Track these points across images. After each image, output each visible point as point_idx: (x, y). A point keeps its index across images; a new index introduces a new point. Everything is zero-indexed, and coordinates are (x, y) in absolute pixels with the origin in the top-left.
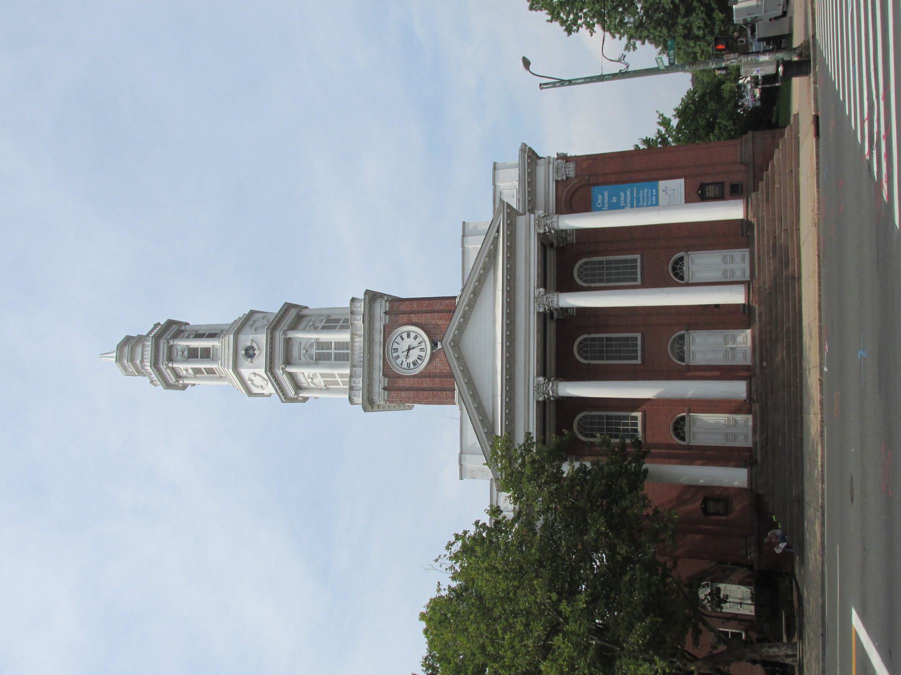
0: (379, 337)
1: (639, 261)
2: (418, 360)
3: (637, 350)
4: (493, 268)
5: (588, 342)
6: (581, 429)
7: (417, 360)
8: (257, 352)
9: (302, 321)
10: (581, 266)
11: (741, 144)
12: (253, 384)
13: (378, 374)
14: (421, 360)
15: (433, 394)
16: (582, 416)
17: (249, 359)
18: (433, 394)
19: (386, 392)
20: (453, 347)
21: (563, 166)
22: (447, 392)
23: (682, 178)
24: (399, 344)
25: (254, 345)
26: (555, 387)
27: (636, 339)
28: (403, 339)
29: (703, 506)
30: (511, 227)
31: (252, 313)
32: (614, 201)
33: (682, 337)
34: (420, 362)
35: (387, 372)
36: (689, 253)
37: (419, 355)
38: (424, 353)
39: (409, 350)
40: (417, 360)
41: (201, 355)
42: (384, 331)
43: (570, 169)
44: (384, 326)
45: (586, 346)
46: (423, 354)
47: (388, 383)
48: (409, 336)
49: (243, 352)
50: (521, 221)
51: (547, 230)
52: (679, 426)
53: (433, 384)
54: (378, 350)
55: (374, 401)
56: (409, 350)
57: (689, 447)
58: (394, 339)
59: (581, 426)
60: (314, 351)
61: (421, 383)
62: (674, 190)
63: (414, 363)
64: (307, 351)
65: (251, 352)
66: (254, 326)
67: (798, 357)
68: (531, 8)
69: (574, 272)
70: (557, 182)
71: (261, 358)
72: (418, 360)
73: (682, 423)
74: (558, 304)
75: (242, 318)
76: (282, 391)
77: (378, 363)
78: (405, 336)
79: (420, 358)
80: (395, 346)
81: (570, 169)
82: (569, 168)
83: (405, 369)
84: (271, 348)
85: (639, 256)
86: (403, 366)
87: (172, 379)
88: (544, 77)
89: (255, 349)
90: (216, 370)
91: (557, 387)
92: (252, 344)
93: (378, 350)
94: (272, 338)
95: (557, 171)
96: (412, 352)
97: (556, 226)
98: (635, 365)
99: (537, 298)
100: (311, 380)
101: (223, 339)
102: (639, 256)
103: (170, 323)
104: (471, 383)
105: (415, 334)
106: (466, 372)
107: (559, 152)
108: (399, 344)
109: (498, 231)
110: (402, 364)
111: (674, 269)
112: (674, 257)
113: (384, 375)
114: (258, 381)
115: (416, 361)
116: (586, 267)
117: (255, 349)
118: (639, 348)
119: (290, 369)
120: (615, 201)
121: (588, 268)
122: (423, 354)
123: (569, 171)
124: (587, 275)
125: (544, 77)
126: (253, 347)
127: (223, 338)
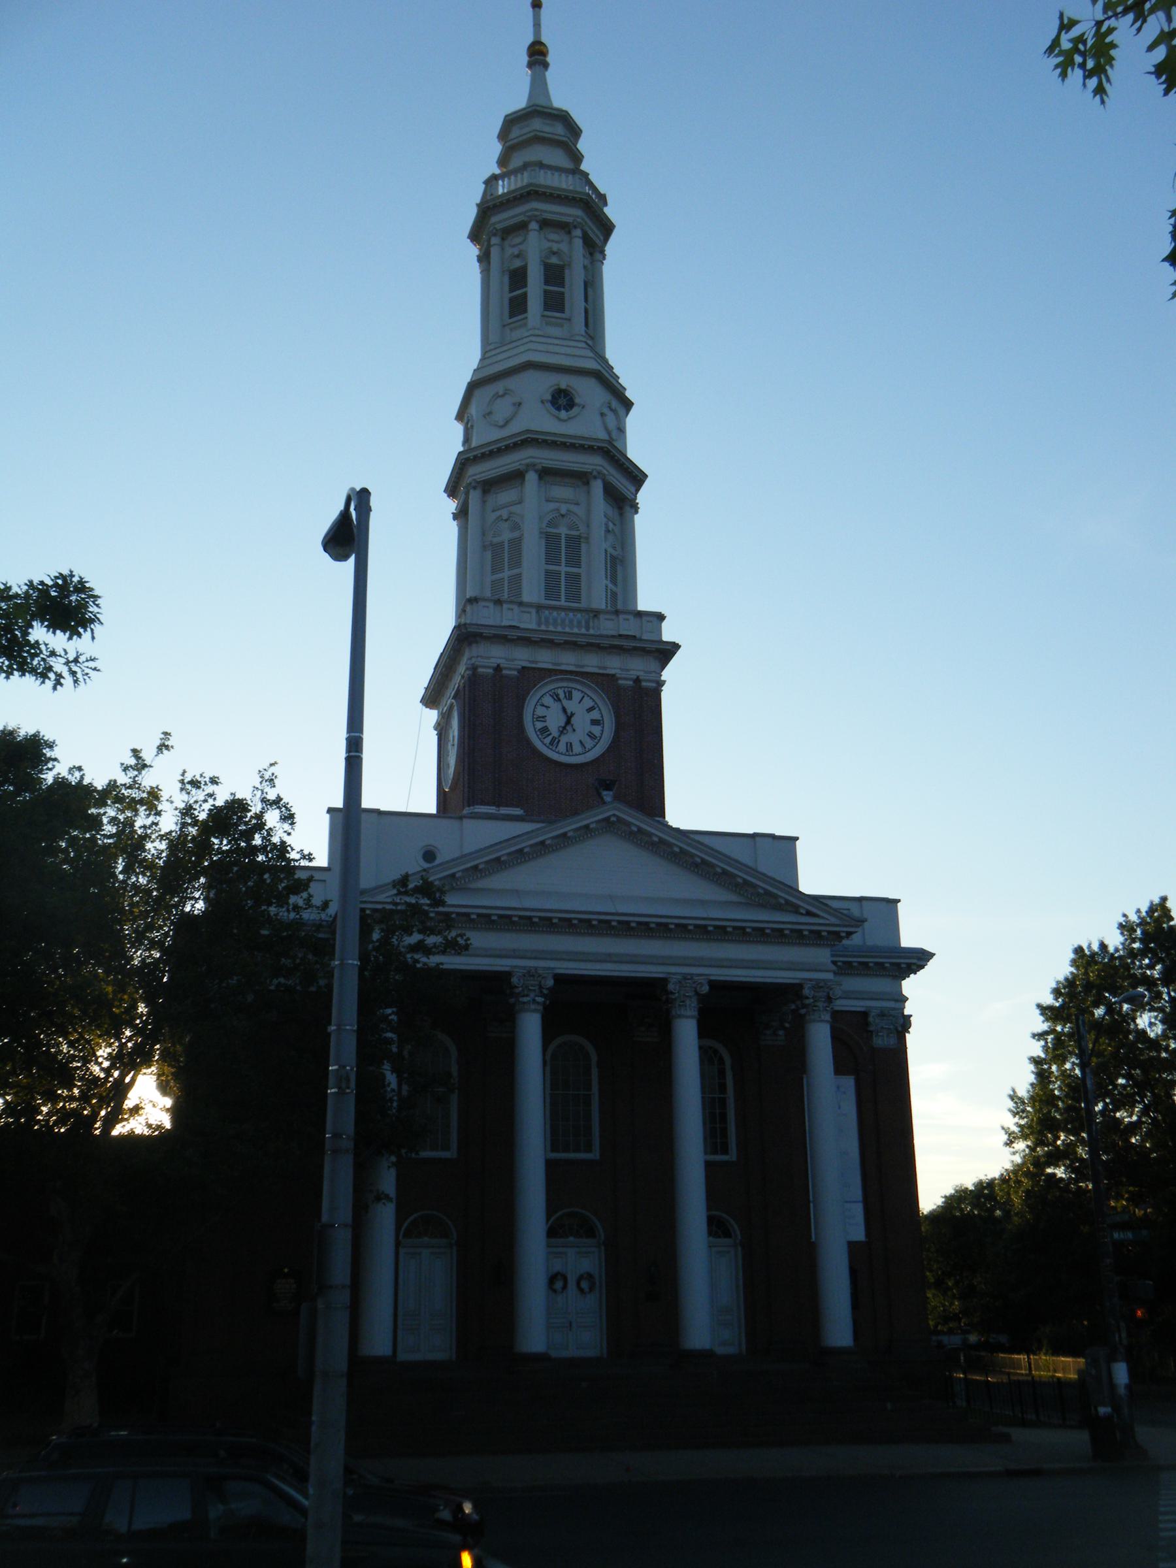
0: (592, 662)
1: (725, 1158)
2: (550, 738)
4: (743, 901)
8: (563, 414)
9: (613, 508)
12: (497, 396)
13: (521, 657)
14: (552, 743)
17: (550, 398)
19: (491, 671)
20: (607, 820)
21: (892, 1027)
24: (580, 703)
25: (575, 410)
26: (533, 1007)
27: (589, 1148)
28: (590, 710)
30: (816, 938)
31: (628, 405)
33: (590, 1232)
35: (531, 677)
36: (740, 1249)
37: (571, 743)
38: (564, 751)
39: (568, 722)
41: (550, 292)
42: (603, 675)
43: (885, 1039)
44: (613, 675)
47: (507, 676)
48: (595, 722)
49: (563, 386)
50: (821, 955)
51: (807, 1002)
54: (568, 660)
55: (474, 645)
56: (568, 722)
58: (589, 694)
60: (563, 531)
64: (563, 516)
65: (562, 401)
66: (606, 410)
68: (1079, 950)
70: (865, 1015)
71: (546, 422)
72: (550, 738)
74: (680, 1016)
75: (618, 382)
76: (483, 455)
77: (545, 658)
78: (595, 715)
80: (577, 695)
81: (885, 1039)
82: (888, 1036)
83: (534, 711)
84: (582, 447)
85: (734, 1159)
87: (500, 219)
88: (354, 746)
89: (567, 411)
90: (524, 319)
91: (535, 1011)
93: (568, 660)
94: (591, 448)
95: (882, 1014)
96: (562, 720)
97: (812, 1017)
99: (691, 979)
100: (505, 517)
101: (583, 345)
102: (734, 1159)
103: (607, 228)
104: (543, 848)
105: (597, 734)
106: (564, 840)
107: (912, 1019)
108: (580, 703)
109: (809, 914)
112: (732, 1222)
113: (523, 668)
114: (503, 409)
117: (567, 411)
123: (883, 1036)
125: (354, 746)
127: (586, 342)
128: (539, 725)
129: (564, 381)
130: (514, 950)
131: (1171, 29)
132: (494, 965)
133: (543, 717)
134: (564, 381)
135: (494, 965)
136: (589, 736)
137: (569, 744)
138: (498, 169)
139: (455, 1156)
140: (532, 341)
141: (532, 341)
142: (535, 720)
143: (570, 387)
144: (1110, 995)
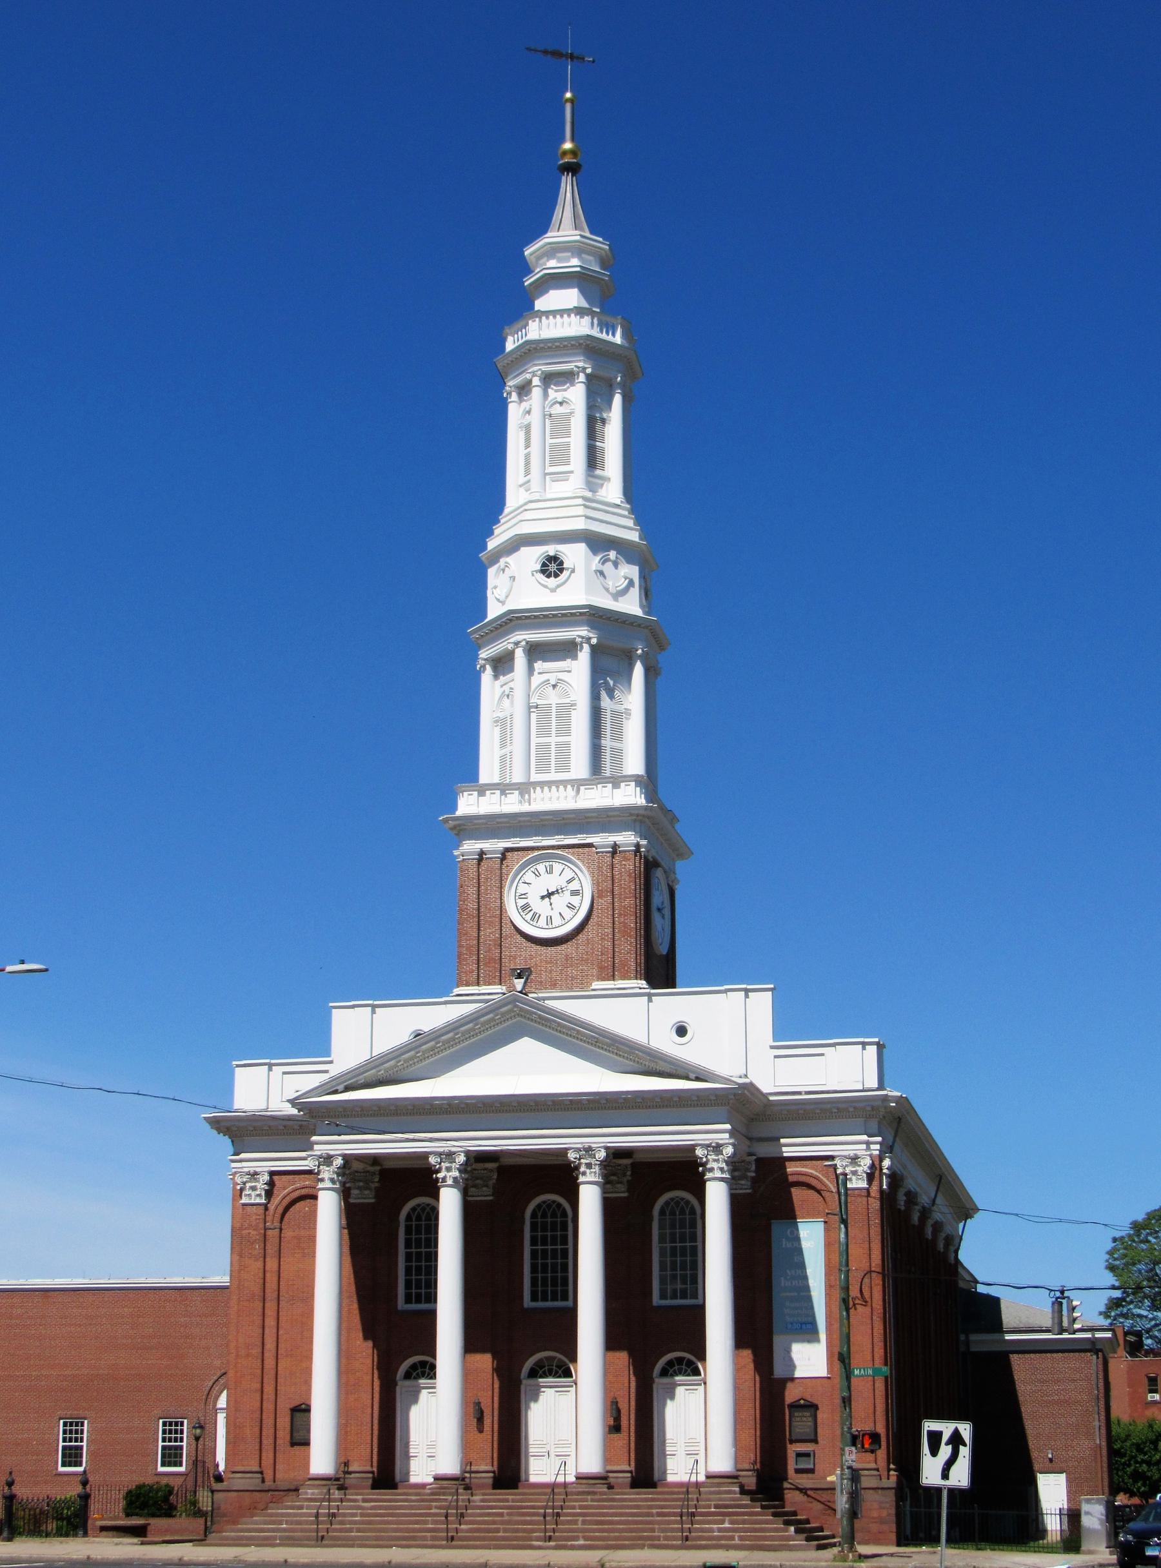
3: (547, 1300)
5: (689, 1215)
6: (419, 1209)
7: (532, 913)
8: (552, 581)
10: (688, 1202)
11: (877, 1470)
14: (532, 919)
15: (472, 947)
16: (566, 1208)
18: (472, 947)
22: (475, 973)
23: (829, 1372)
25: (565, 574)
29: (802, 1402)
32: (795, 1258)
34: (528, 917)
37: (540, 915)
40: (532, 913)
45: (554, 1215)
46: (542, 922)
49: (552, 554)
52: (427, 1370)
53: (490, 945)
57: (652, 1381)
59: (549, 1206)
61: (490, 922)
62: (809, 1359)
63: (526, 907)
65: (553, 567)
67: (303, 1542)
69: (427, 1198)
73: (689, 1371)
79: (536, 917)
86: (521, 885)
92: (567, 569)
98: (521, 1297)
105: (577, 905)
110: (525, 883)
111: (680, 1360)
115: (531, 911)
116: (539, 1215)
118: (549, 1304)
119: (520, 657)
120: (796, 1260)
121: (412, 1221)
122: (542, 922)
124: (673, 1213)
126: (561, 570)
128: (521, 902)
129: (551, 550)
130: (614, 1427)
131: (647, 987)
132: (755, 1416)
133: (524, 894)
134: (551, 550)
135: (755, 1416)
136: (569, 907)
137: (549, 918)
138: (508, 340)
139: (526, 1306)
140: (526, 510)
141: (526, 510)
142: (517, 898)
143: (567, 398)
144: (227, 1408)
